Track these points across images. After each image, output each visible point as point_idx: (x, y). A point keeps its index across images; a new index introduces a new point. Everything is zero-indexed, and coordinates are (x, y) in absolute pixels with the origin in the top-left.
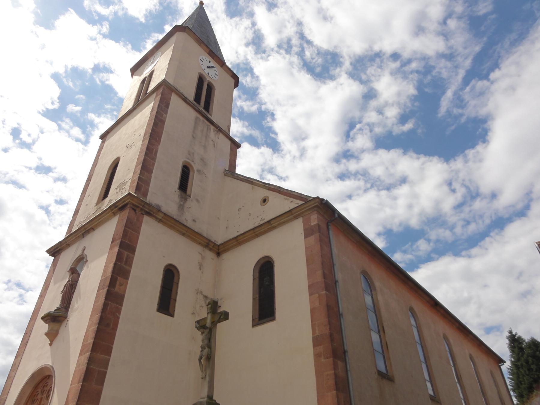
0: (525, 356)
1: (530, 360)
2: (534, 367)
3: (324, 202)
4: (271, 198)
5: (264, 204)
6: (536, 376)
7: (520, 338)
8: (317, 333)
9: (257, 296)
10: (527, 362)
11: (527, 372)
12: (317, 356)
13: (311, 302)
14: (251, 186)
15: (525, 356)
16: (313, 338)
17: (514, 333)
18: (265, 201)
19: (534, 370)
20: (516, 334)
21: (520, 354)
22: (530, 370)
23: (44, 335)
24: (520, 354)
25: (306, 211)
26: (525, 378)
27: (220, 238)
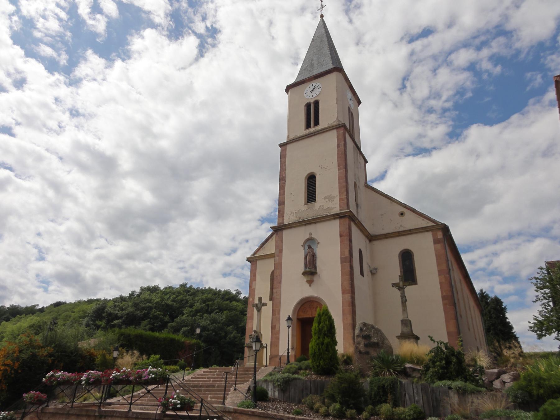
0: (489, 308)
1: (492, 311)
2: (494, 316)
3: (446, 226)
4: (406, 214)
5: (401, 216)
6: (494, 322)
7: (487, 295)
8: (444, 294)
9: (402, 270)
10: (490, 312)
11: (489, 318)
12: (444, 305)
13: (440, 279)
14: (389, 201)
15: (489, 308)
16: (442, 296)
17: (483, 292)
18: (402, 214)
19: (494, 318)
20: (485, 292)
21: (486, 306)
22: (491, 317)
23: (306, 283)
24: (486, 306)
25: (435, 229)
26: (486, 322)
27: (372, 230)
